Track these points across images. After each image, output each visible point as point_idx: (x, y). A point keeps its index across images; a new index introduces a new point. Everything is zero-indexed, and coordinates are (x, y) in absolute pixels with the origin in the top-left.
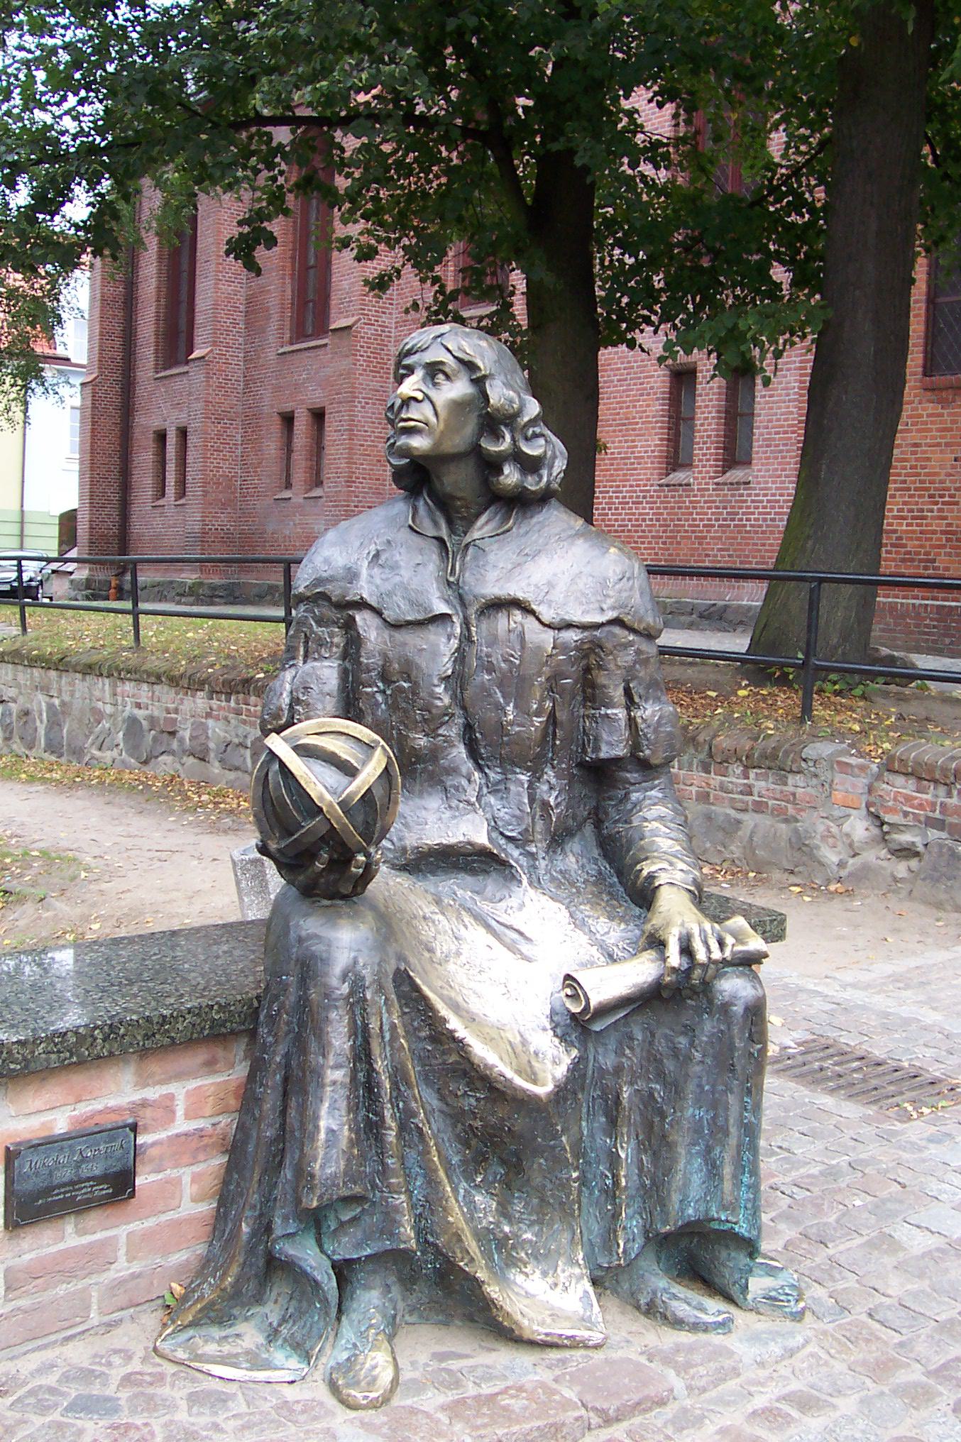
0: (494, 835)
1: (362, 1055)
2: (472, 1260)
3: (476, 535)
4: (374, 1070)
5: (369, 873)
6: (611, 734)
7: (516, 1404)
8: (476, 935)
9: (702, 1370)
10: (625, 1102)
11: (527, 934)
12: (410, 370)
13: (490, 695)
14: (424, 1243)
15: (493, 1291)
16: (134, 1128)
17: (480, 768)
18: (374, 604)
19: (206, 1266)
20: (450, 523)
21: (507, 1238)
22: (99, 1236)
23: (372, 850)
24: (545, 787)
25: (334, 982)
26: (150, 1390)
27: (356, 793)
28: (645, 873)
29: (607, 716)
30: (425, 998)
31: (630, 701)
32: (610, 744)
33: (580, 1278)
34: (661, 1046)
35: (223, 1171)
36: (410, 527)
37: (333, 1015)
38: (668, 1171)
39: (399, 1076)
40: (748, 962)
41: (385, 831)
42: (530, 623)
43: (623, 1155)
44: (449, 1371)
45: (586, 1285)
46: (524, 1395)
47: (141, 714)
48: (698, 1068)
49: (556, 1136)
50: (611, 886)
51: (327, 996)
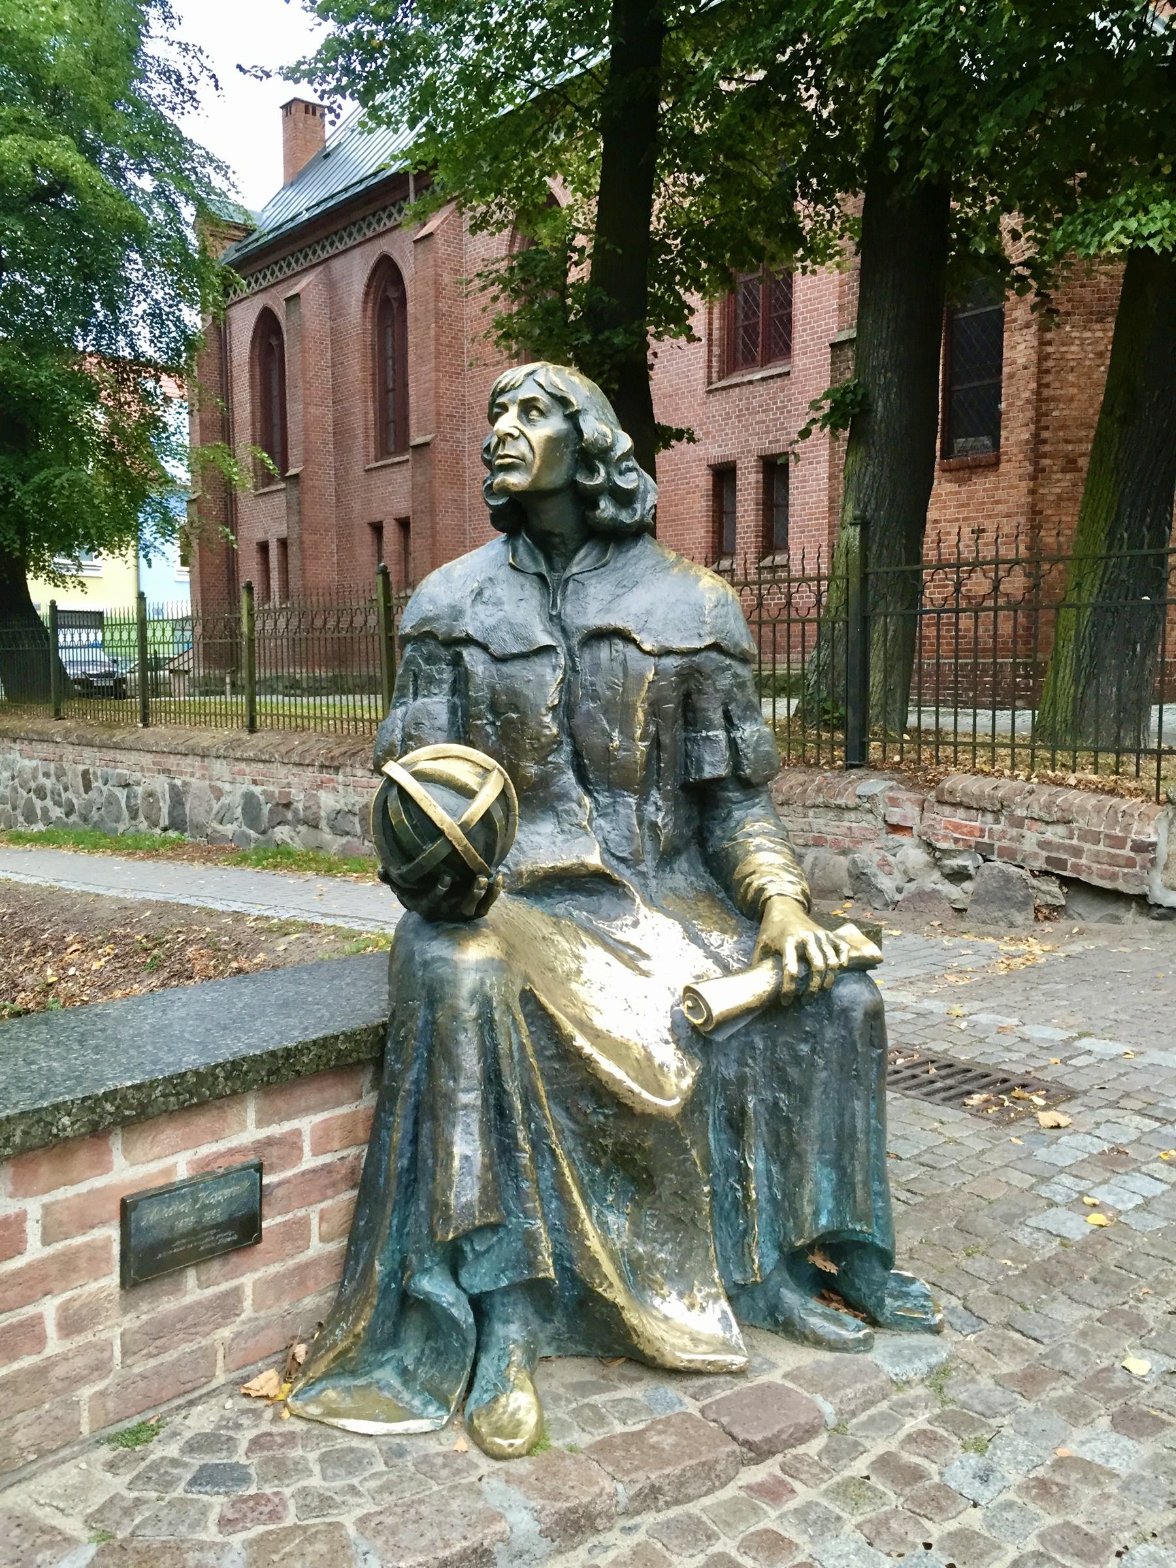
0: (606, 857)
1: (492, 1078)
2: (611, 1285)
3: (575, 570)
4: (505, 1091)
5: (491, 894)
6: (713, 755)
7: (668, 1441)
8: (595, 956)
9: (850, 1392)
10: (751, 1113)
11: (645, 950)
12: (504, 408)
13: (596, 722)
14: (561, 1269)
15: (632, 1317)
16: (259, 1168)
17: (589, 793)
18: (480, 640)
19: (341, 1308)
20: (549, 560)
21: (640, 1257)
22: (225, 1286)
23: (493, 871)
24: (652, 809)
25: (463, 1004)
26: (278, 1453)
27: (474, 814)
28: (755, 885)
29: (708, 737)
30: (551, 1017)
31: (729, 723)
32: (712, 764)
33: (716, 1298)
34: (783, 1054)
35: (353, 1206)
36: (513, 567)
37: (462, 1037)
38: (799, 1182)
39: (529, 1096)
40: (861, 967)
41: (503, 856)
42: (631, 651)
43: (751, 1166)
44: (593, 1407)
45: (724, 1304)
46: (672, 1430)
47: (257, 790)
48: (824, 1074)
49: (686, 1151)
50: (722, 900)
51: (455, 1018)
